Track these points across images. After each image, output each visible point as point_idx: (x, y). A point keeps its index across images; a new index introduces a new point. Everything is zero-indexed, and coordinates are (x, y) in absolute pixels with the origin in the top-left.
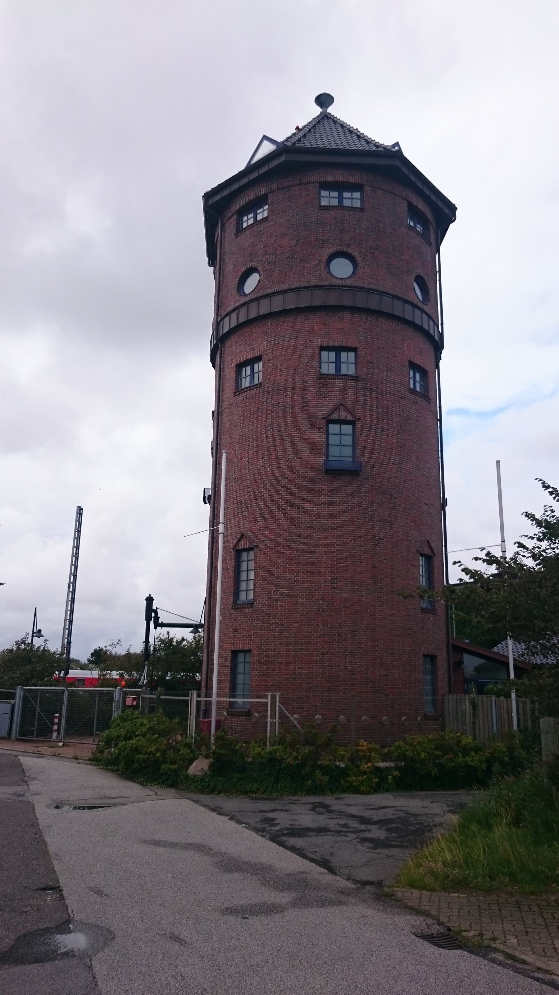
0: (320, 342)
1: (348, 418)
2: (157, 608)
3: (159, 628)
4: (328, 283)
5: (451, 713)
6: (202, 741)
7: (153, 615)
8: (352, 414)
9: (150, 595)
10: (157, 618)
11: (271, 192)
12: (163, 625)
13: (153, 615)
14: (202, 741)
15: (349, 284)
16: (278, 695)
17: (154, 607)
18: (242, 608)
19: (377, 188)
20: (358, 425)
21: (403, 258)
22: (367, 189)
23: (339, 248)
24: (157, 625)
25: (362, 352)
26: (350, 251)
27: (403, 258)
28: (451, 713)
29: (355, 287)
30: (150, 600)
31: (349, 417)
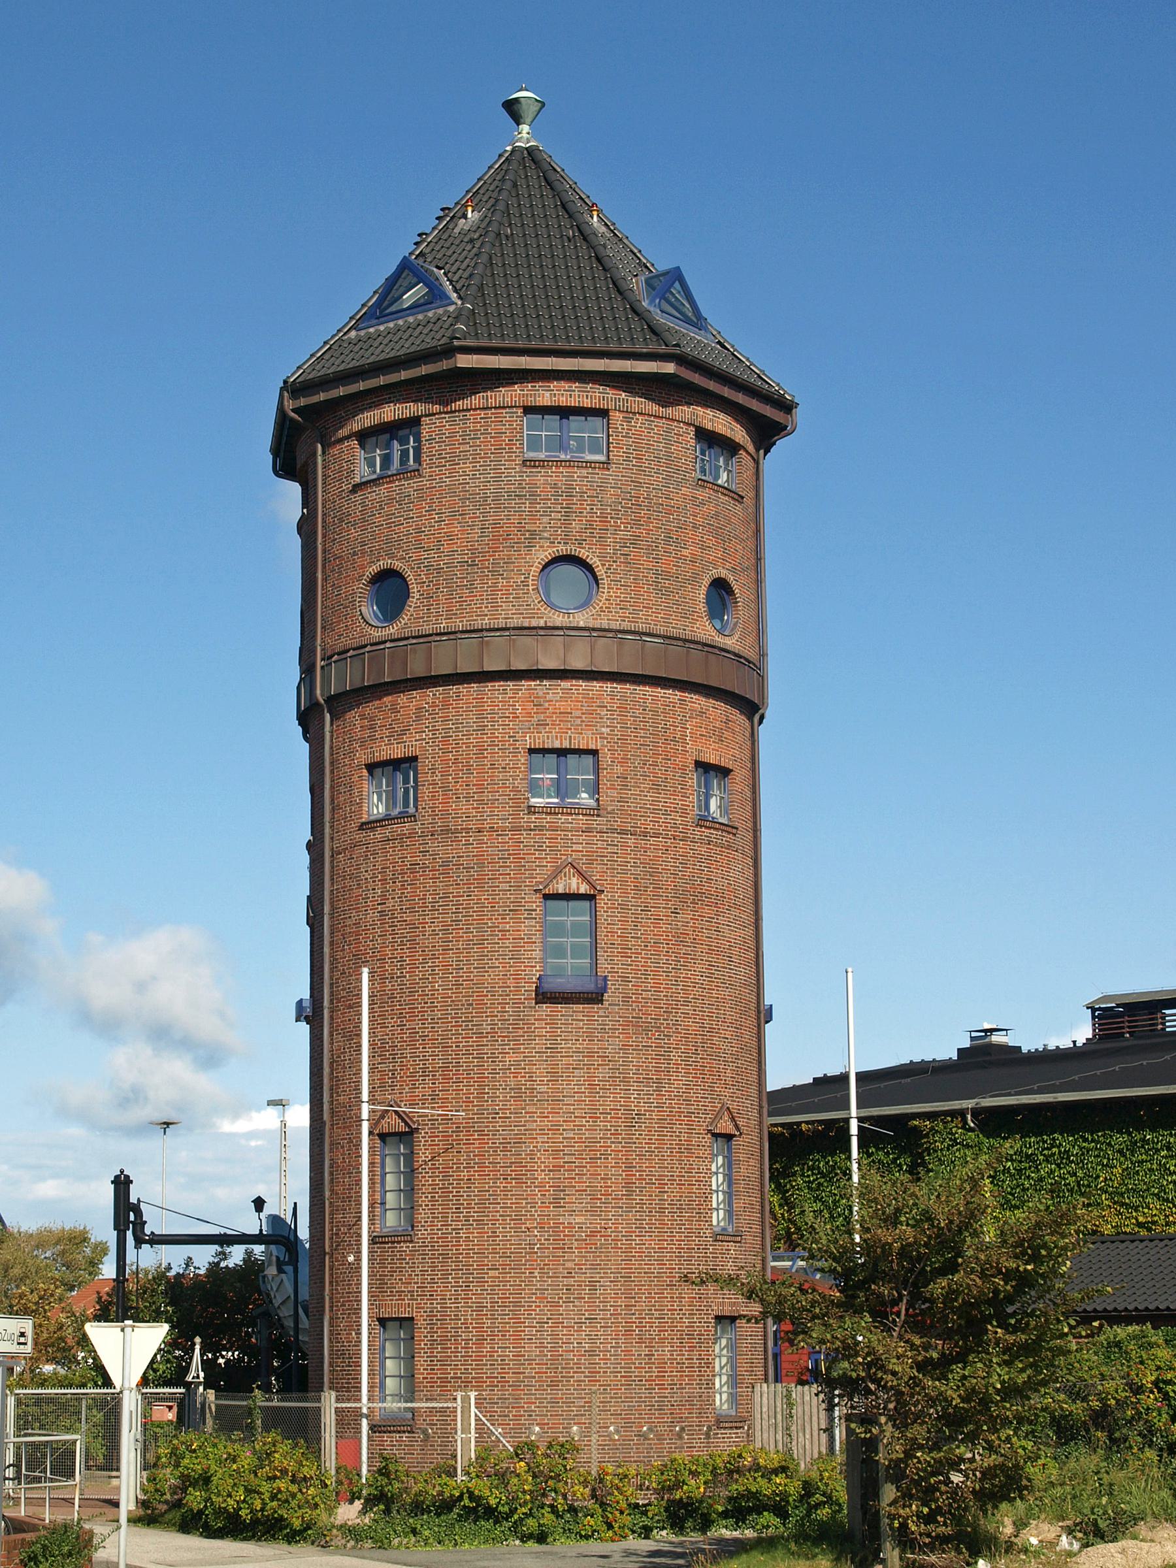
0: (529, 742)
1: (582, 891)
2: (139, 1200)
3: (145, 1247)
4: (542, 624)
5: (765, 1416)
6: (348, 1471)
7: (132, 1217)
8: (589, 882)
9: (122, 1172)
10: (140, 1224)
11: (426, 416)
12: (158, 1240)
13: (132, 1217)
14: (348, 1471)
15: (582, 624)
16: (473, 1395)
17: (133, 1200)
18: (393, 1242)
19: (634, 413)
20: (602, 900)
21: (685, 552)
22: (617, 417)
23: (563, 549)
24: (139, 1242)
25: (606, 758)
26: (583, 553)
27: (685, 552)
28: (765, 1416)
29: (594, 629)
30: (122, 1184)
31: (584, 889)
